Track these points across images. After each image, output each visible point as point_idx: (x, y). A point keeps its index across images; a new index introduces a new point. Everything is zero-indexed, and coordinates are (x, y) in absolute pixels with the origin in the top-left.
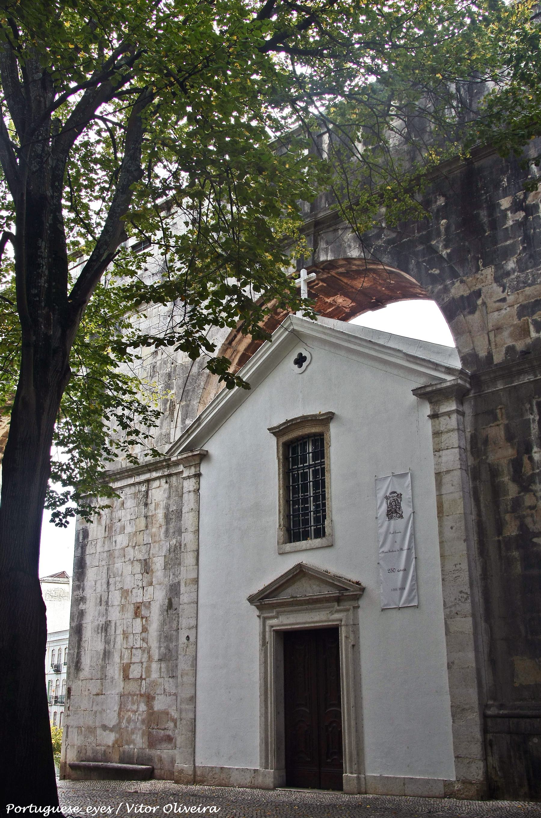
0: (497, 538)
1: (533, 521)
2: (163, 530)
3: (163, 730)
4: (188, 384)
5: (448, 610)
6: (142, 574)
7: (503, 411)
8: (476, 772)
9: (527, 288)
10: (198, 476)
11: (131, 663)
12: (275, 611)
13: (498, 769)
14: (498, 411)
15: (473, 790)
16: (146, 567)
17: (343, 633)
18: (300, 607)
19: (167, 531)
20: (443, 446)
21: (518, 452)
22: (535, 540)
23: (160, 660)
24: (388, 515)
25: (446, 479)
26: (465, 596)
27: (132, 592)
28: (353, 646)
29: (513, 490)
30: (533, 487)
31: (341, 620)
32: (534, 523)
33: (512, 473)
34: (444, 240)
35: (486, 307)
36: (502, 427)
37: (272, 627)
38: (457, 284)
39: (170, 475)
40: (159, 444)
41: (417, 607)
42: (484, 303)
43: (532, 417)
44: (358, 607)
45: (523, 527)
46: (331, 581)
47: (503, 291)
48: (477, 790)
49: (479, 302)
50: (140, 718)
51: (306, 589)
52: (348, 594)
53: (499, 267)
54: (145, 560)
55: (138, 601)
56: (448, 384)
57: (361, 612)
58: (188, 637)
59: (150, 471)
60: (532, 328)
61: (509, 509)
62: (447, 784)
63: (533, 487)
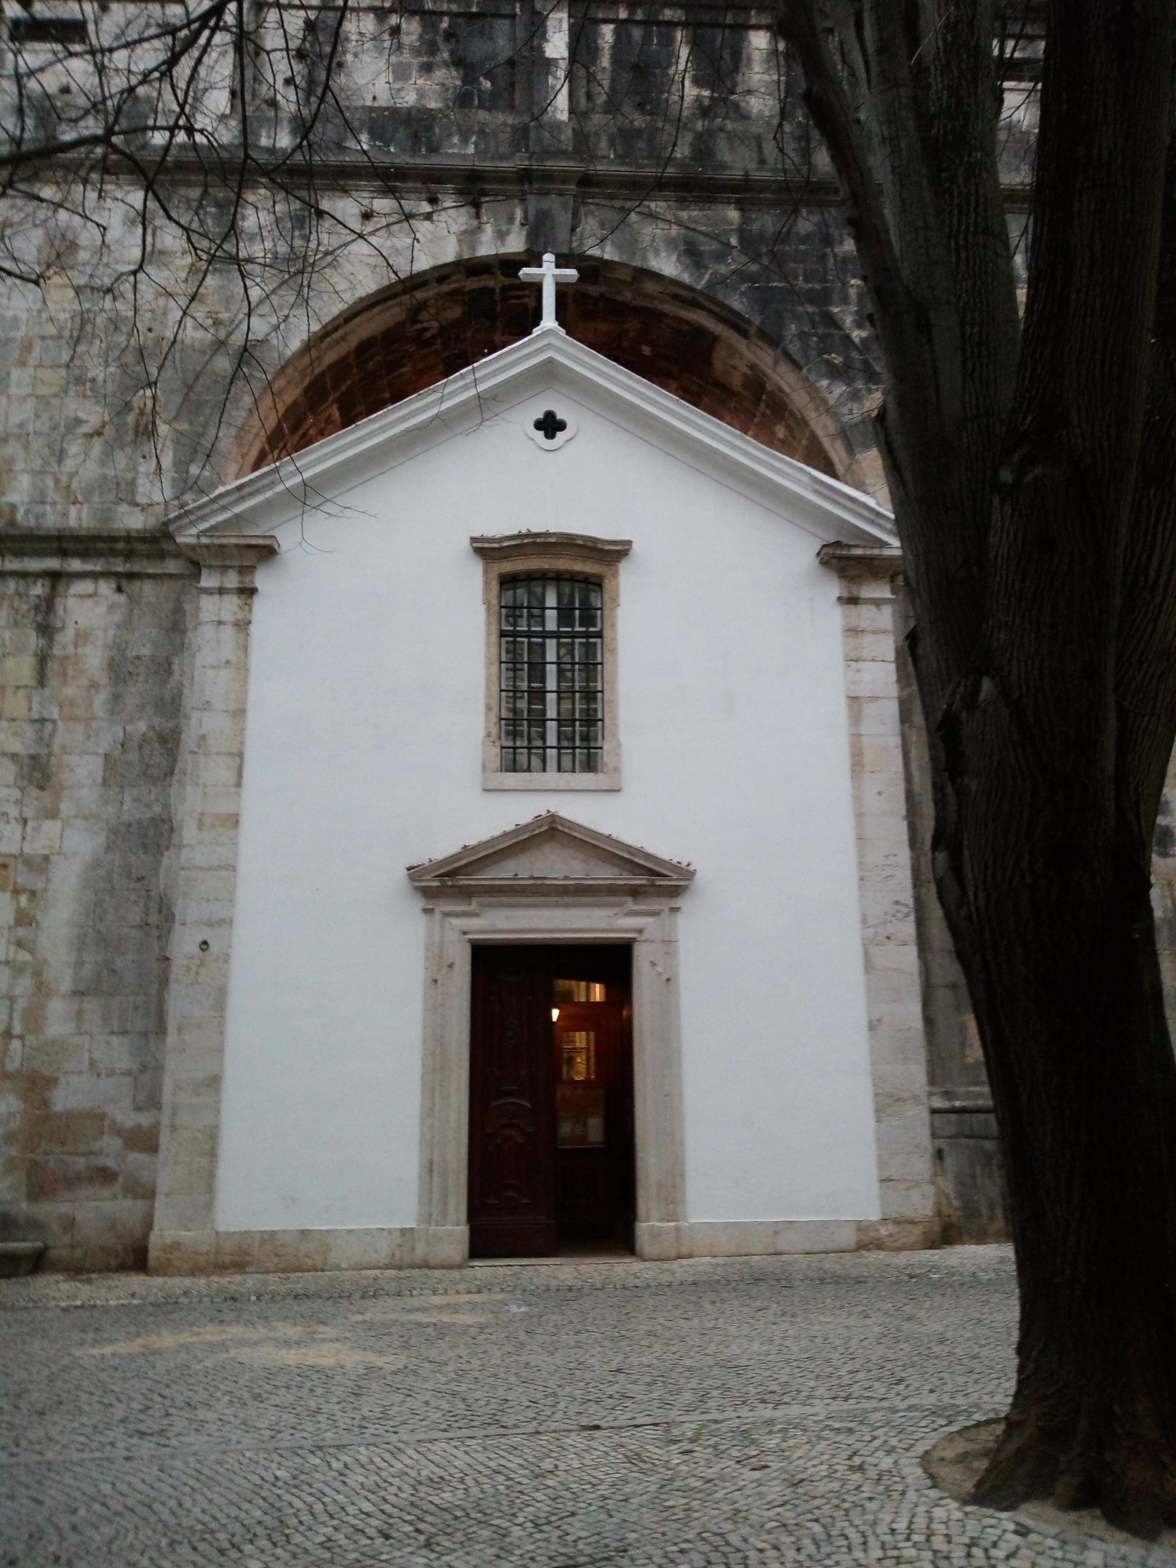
2: (100, 701)
3: (84, 1155)
5: (871, 931)
6: (22, 790)
8: (921, 1203)
10: (248, 592)
12: (474, 901)
15: (916, 1233)
18: (543, 899)
19: (116, 698)
20: (864, 654)
23: (78, 994)
25: (870, 710)
26: (905, 910)
28: (668, 980)
34: (857, 312)
37: (465, 933)
39: (131, 576)
40: (96, 499)
46: (627, 856)
51: (555, 865)
52: (656, 882)
54: (33, 757)
57: (681, 920)
58: (205, 943)
59: (63, 553)
62: (861, 1227)
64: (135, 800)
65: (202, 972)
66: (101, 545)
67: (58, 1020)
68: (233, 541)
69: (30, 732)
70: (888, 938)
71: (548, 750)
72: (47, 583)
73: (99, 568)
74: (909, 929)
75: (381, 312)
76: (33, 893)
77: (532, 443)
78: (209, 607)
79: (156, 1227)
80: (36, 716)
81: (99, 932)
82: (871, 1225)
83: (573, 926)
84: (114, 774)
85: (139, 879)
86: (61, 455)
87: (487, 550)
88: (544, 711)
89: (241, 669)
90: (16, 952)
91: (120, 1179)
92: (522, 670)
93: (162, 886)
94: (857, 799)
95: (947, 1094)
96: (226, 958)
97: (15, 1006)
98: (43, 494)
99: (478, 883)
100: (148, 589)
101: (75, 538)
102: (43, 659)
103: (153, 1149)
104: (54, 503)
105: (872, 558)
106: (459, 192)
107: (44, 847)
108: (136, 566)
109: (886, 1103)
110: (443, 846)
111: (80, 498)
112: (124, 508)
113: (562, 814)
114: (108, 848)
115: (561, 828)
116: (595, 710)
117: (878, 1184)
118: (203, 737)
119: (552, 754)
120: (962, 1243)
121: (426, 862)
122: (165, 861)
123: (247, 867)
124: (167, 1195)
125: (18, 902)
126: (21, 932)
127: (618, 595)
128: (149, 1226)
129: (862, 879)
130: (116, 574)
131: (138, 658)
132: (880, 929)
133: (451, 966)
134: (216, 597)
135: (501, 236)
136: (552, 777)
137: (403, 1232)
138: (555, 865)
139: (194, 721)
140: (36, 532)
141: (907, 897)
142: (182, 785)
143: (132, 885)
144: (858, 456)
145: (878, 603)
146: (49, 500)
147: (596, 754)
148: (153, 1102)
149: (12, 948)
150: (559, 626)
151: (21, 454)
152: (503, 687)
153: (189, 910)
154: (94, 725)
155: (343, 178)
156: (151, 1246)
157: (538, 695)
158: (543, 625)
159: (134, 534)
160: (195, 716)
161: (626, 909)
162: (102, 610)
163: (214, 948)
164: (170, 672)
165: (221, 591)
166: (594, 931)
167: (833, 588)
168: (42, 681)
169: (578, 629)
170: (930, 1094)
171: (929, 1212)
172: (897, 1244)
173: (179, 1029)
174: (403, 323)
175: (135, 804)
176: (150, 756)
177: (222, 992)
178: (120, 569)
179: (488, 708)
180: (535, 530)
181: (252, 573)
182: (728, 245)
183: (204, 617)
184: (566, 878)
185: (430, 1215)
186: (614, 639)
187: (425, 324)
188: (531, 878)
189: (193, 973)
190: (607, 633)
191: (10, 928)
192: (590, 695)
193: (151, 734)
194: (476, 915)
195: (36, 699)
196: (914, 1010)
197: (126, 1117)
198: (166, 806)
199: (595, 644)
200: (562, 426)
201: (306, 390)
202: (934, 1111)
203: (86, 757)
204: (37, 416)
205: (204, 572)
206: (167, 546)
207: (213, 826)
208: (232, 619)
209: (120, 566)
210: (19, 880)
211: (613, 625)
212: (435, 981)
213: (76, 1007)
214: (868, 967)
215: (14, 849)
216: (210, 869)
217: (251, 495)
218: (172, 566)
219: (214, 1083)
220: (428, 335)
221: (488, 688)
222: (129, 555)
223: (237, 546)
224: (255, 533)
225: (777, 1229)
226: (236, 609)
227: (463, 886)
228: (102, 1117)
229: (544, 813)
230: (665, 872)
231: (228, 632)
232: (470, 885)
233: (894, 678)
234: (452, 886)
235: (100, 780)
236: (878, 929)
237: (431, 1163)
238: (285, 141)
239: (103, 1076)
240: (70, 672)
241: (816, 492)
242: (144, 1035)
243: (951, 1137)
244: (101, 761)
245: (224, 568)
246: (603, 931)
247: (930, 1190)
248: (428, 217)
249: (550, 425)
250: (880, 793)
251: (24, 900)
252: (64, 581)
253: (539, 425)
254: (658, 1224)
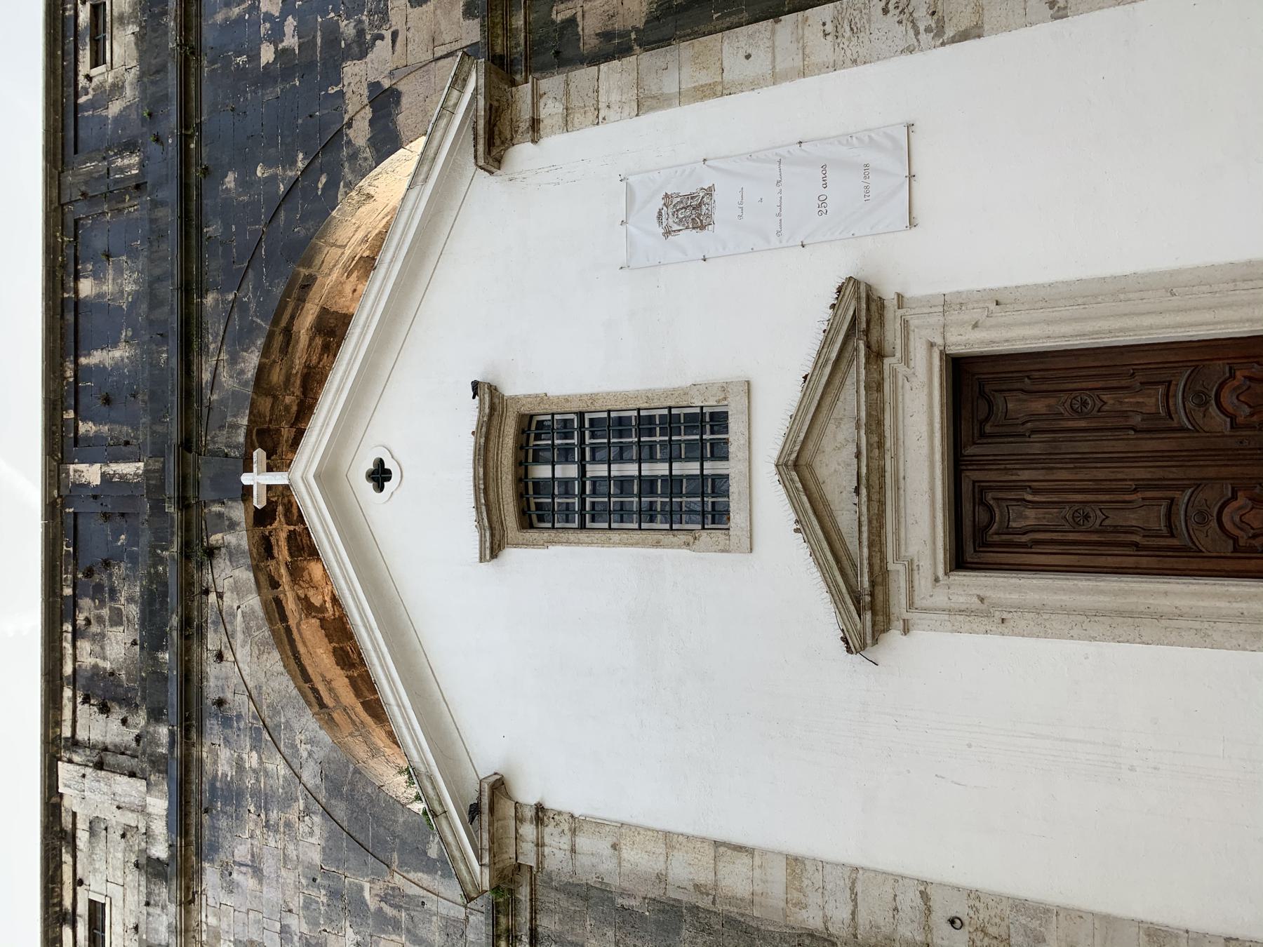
4: (361, 838)
5: (923, 36)
12: (891, 567)
24: (702, 227)
31: (932, 345)
37: (937, 580)
38: (351, 133)
41: (910, 126)
44: (900, 297)
51: (837, 468)
52: (862, 325)
57: (915, 291)
58: (952, 922)
75: (304, 643)
83: (925, 435)
87: (493, 547)
94: (754, 84)
96: (974, 895)
106: (200, 566)
127: (537, 396)
129: (855, 62)
135: (232, 526)
145: (537, 96)
150: (573, 462)
155: (189, 678)
157: (648, 484)
161: (901, 368)
163: (961, 910)
166: (931, 407)
169: (575, 441)
174: (322, 620)
181: (521, 805)
182: (234, 301)
186: (581, 398)
187: (327, 599)
192: (645, 424)
199: (591, 420)
216: (855, 901)
219: (668, 837)
230: (849, 317)
236: (922, 29)
238: (163, 731)
241: (426, 180)
246: (930, 395)
248: (220, 596)
249: (380, 476)
250: (748, 57)
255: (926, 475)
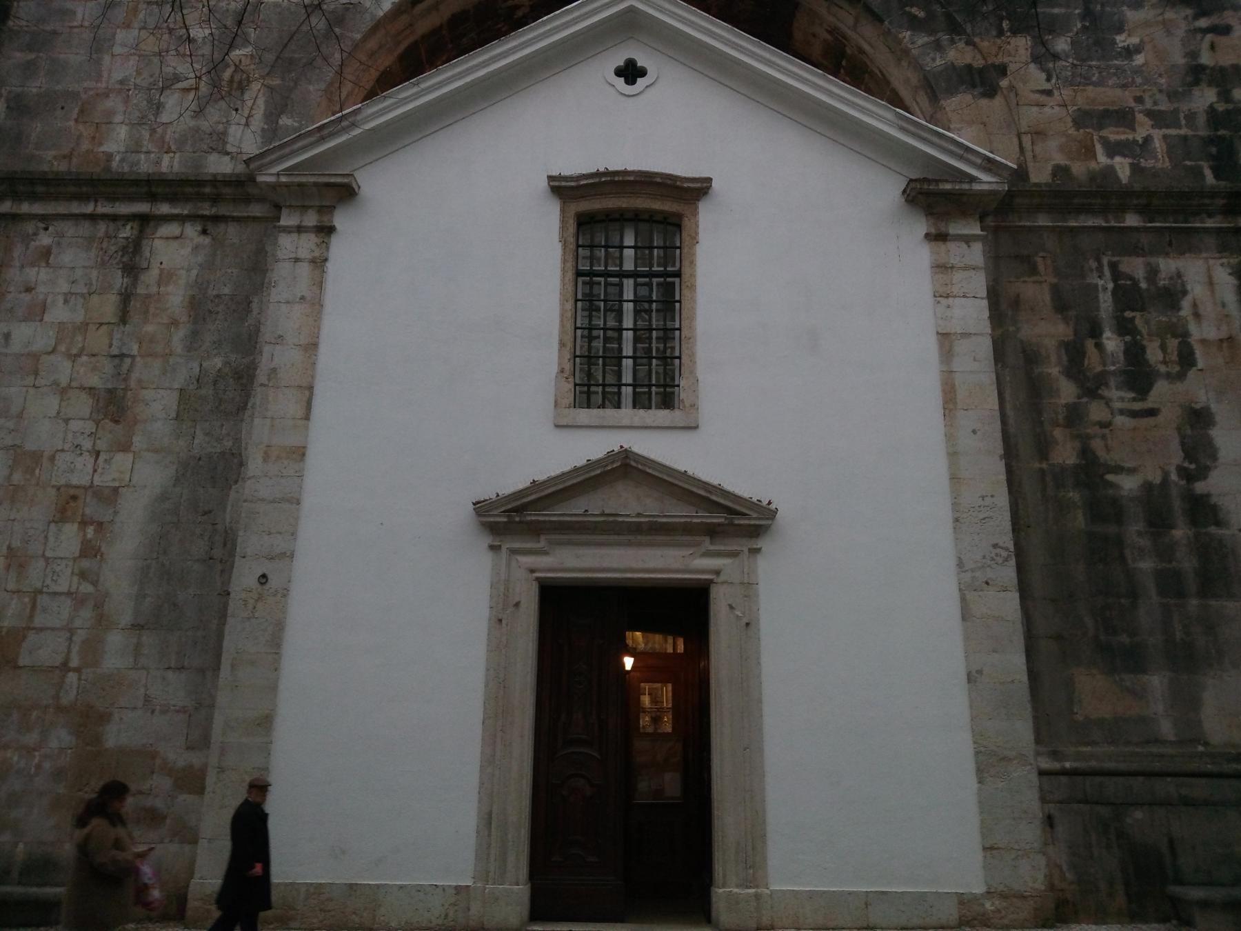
0: (1037, 465)
1: (1106, 446)
2: (179, 335)
5: (969, 575)
6: (97, 423)
7: (1049, 262)
9: (1090, 88)
10: (327, 231)
11: (29, 628)
12: (543, 538)
13: (1065, 867)
14: (1039, 260)
16: (113, 406)
17: (720, 600)
19: (195, 334)
20: (955, 290)
21: (1076, 333)
22: (1110, 477)
23: (137, 627)
25: (961, 347)
26: (1004, 554)
27: (52, 459)
28: (747, 624)
29: (1067, 391)
30: (1105, 392)
32: (1108, 449)
33: (1066, 363)
35: (1017, 95)
36: (1046, 287)
37: (532, 571)
38: (961, 45)
39: (216, 219)
40: (188, 148)
42: (1012, 87)
43: (1101, 283)
44: (758, 550)
45: (1085, 452)
47: (1048, 80)
48: (1036, 909)
49: (1004, 83)
50: (47, 765)
51: (628, 502)
52: (736, 522)
53: (1040, 41)
54: (111, 392)
55: (75, 482)
56: (986, 187)
58: (264, 576)
59: (153, 198)
60: (1099, 149)
61: (1061, 421)
63: (1105, 392)
64: (207, 434)
65: (260, 605)
66: (189, 190)
67: (116, 652)
68: (312, 179)
69: (108, 367)
70: (987, 583)
71: (624, 388)
72: (136, 225)
73: (186, 212)
74: (1009, 573)
76: (100, 524)
77: (611, 89)
78: (287, 244)
79: (197, 875)
80: (115, 351)
81: (163, 565)
82: (975, 898)
83: (647, 566)
84: (188, 409)
85: (205, 513)
86: (159, 107)
87: (564, 189)
88: (620, 350)
89: (315, 305)
90: (79, 584)
91: (168, 821)
92: (598, 337)
93: (228, 520)
94: (950, 437)
95: (1055, 755)
96: (285, 593)
97: (74, 638)
98: (138, 143)
99: (547, 518)
100: (232, 232)
101: (163, 181)
102: (126, 297)
103: (201, 790)
104: (148, 152)
105: (962, 194)
107: (114, 480)
108: (223, 210)
109: (989, 762)
110: (513, 480)
111: (173, 148)
112: (213, 157)
113: (636, 449)
114: (177, 481)
115: (633, 464)
116: (673, 348)
117: (979, 855)
118: (274, 370)
119: (627, 391)
120: (1078, 922)
121: (494, 497)
122: (233, 494)
123: (310, 500)
124: (210, 841)
125: (85, 535)
126: (85, 564)
127: (697, 234)
128: (191, 875)
129: (957, 520)
130: (202, 217)
131: (218, 296)
132: (978, 574)
133: (517, 605)
134: (295, 236)
136: (627, 414)
137: (458, 889)
138: (628, 502)
139: (266, 356)
140: (126, 177)
141: (1008, 541)
142: (252, 417)
143: (200, 519)
144: (942, 102)
145: (968, 240)
146: (144, 149)
147: (673, 393)
148: (204, 742)
149: (75, 579)
151: (120, 107)
152: (579, 325)
153: (251, 542)
154: (171, 361)
156: (189, 896)
158: (621, 265)
159: (219, 178)
160: (267, 349)
162: (186, 251)
163: (274, 582)
164: (248, 310)
165: (300, 229)
167: (921, 226)
168: (124, 319)
170: (1038, 754)
171: (1040, 885)
172: (1006, 921)
173: (233, 666)
175: (207, 439)
176: (225, 391)
177: (279, 627)
178: (207, 213)
179: (562, 344)
180: (613, 167)
183: (280, 254)
184: (639, 515)
185: (488, 872)
188: (603, 514)
189: (250, 607)
190: (686, 271)
191: (75, 559)
192: (668, 334)
193: (227, 370)
194: (546, 553)
195: (117, 336)
196: (1018, 660)
197: (177, 756)
198: (237, 440)
200: (642, 73)
201: (402, 58)
202: (1042, 773)
203: (161, 391)
204: (139, 73)
205: (285, 212)
206: (252, 190)
207: (278, 457)
208: (309, 257)
209: (207, 210)
210: (88, 511)
211: (692, 263)
212: (500, 621)
213: (135, 640)
214: (966, 615)
215: (85, 480)
216: (274, 501)
217: (332, 135)
218: (256, 210)
219: (265, 723)
220: (520, 13)
221: (562, 325)
222: (215, 199)
223: (316, 184)
224: (336, 172)
225: (868, 900)
226: (314, 247)
227: (532, 522)
228: (154, 755)
229: (617, 449)
231: (304, 270)
232: (539, 522)
233: (986, 314)
234: (520, 522)
235: (173, 415)
237: (490, 814)
239: (157, 713)
240: (152, 310)
241: (902, 129)
242: (202, 671)
243: (1061, 802)
244: (176, 395)
245: (304, 208)
246: (677, 571)
247: (1041, 861)
249: (631, 72)
250: (974, 432)
251: (90, 531)
252: (152, 224)
253: (619, 72)
254: (736, 890)
255: (615, 565)
